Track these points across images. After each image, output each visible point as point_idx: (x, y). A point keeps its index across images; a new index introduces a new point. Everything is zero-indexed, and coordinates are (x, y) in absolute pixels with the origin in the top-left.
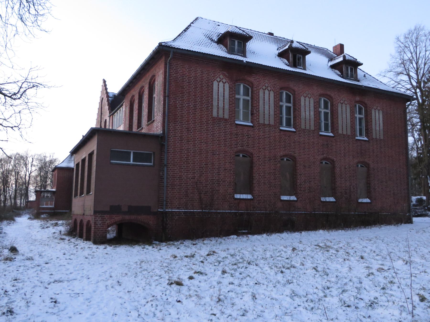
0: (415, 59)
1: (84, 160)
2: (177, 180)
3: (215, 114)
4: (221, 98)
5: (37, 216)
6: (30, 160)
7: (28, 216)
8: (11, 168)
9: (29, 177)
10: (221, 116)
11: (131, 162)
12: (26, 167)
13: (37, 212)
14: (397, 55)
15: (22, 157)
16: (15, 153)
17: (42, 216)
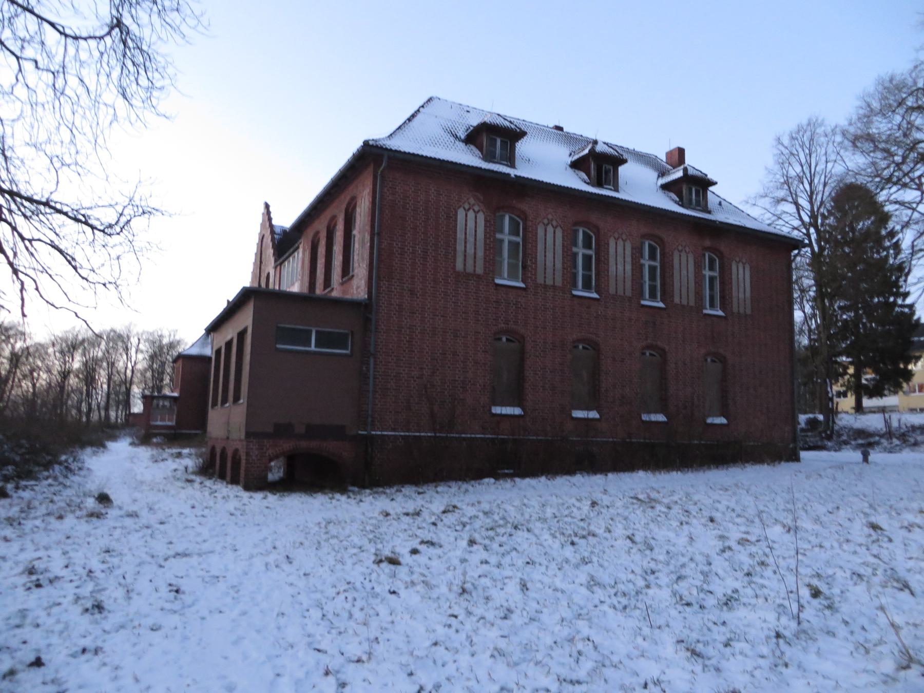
0: (808, 175)
1: (229, 344)
3: (459, 266)
4: (471, 239)
5: (145, 440)
6: (134, 341)
7: (129, 440)
8: (100, 354)
9: (133, 371)
10: (470, 269)
11: (313, 348)
12: (127, 354)
13: (145, 432)
14: (777, 168)
15: (120, 336)
16: (108, 328)
17: (155, 440)
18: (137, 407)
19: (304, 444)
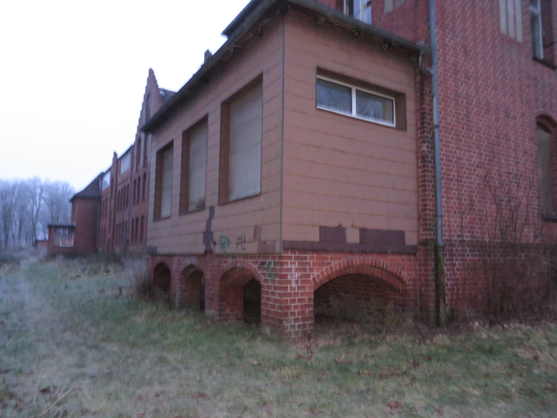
2: (453, 166)
9: (37, 212)
11: (354, 114)
18: (41, 236)
19: (357, 260)
